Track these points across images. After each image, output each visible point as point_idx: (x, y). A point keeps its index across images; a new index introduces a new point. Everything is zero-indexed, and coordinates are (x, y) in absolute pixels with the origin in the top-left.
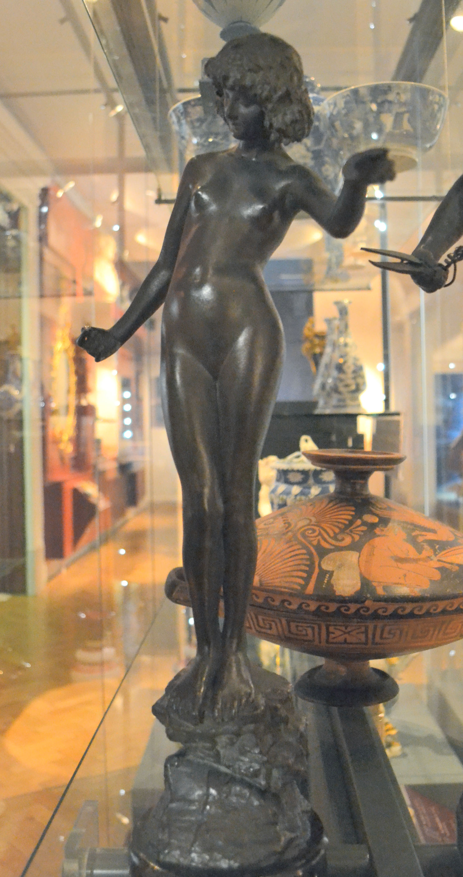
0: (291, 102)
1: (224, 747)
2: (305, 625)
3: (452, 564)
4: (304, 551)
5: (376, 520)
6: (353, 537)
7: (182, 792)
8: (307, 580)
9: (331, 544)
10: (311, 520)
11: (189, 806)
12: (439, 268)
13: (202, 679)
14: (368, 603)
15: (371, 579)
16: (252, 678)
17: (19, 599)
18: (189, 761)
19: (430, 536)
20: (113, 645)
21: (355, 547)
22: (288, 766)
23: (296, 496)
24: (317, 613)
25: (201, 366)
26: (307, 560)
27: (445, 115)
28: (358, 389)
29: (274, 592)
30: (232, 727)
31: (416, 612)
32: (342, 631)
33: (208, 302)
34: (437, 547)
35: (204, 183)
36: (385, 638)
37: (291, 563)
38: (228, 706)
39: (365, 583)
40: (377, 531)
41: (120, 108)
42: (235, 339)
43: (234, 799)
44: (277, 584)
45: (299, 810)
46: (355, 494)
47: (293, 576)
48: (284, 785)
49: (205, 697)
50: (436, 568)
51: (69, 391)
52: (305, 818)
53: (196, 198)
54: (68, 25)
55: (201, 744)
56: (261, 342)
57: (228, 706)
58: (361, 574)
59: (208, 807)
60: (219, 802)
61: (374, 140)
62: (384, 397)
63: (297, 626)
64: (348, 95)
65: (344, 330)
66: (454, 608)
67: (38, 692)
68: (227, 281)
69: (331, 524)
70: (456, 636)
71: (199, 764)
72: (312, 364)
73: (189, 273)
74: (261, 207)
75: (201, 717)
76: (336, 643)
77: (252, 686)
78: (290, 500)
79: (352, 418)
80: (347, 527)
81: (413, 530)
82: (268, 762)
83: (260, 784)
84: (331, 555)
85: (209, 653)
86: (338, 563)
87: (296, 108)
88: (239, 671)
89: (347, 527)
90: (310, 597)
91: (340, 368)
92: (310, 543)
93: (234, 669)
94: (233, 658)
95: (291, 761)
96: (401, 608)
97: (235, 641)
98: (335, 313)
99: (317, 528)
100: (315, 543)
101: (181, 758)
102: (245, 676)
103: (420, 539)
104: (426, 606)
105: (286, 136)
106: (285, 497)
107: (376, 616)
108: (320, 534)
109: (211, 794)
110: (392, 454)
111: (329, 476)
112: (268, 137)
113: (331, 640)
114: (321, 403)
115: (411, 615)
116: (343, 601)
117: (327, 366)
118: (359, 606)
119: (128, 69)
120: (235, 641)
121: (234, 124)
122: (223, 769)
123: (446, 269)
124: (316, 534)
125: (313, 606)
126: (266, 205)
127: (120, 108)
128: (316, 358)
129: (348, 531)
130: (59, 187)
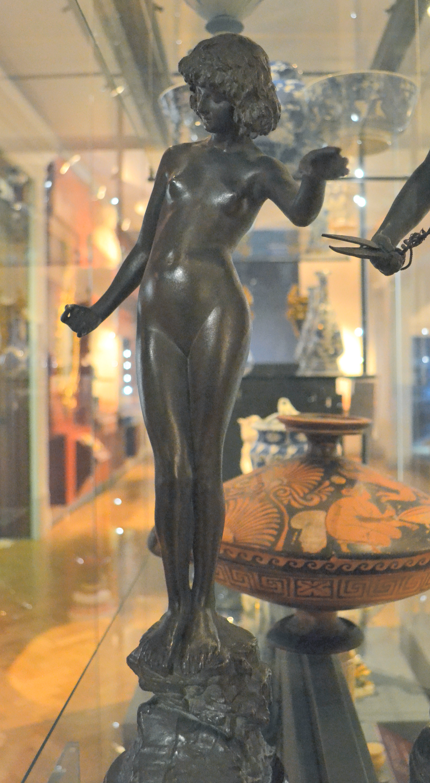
0: (258, 98)
1: (192, 697)
2: (276, 579)
3: (413, 523)
4: (276, 510)
5: (343, 481)
6: (321, 498)
7: (152, 738)
8: (277, 537)
10: (283, 482)
11: (159, 750)
12: (397, 253)
13: (172, 632)
14: (333, 560)
15: (336, 537)
16: (219, 632)
17: (23, 543)
18: (160, 709)
19: (394, 497)
20: (109, 588)
21: (324, 506)
22: (251, 715)
23: (274, 455)
24: (287, 568)
25: (172, 342)
26: (278, 518)
27: (415, 101)
28: (337, 354)
29: (246, 548)
30: (198, 678)
31: (378, 568)
33: (181, 284)
34: (399, 507)
35: (178, 174)
36: (349, 593)
37: (263, 522)
38: (196, 658)
39: (331, 541)
40: (344, 491)
41: (120, 90)
42: (205, 318)
43: (201, 745)
44: (250, 541)
45: (261, 756)
46: (325, 456)
47: (264, 534)
48: (247, 733)
49: (174, 651)
50: (396, 527)
51: (72, 352)
52: (268, 763)
53: (171, 185)
54: (70, 15)
55: (170, 694)
56: (229, 321)
57: (196, 658)
58: (327, 532)
59: (177, 752)
60: (187, 748)
62: (362, 360)
63: (268, 581)
64: (325, 84)
65: (324, 298)
66: (413, 564)
67: (39, 631)
68: (199, 264)
70: (415, 591)
71: (168, 712)
72: (295, 328)
73: (163, 256)
74: (230, 195)
75: (170, 670)
76: (303, 596)
77: (219, 640)
78: (268, 459)
79: (332, 381)
80: (316, 487)
81: (378, 491)
82: (232, 711)
83: (225, 731)
84: (300, 514)
85: (179, 609)
87: (262, 104)
88: (207, 626)
89: (316, 487)
90: (279, 554)
91: (320, 334)
92: (281, 502)
93: (202, 625)
94: (201, 614)
95: (254, 711)
96: (364, 564)
97: (203, 599)
98: (315, 282)
99: (288, 489)
100: (286, 502)
101: (152, 706)
102: (212, 630)
103: (384, 500)
104: (387, 563)
105: (254, 130)
106: (264, 456)
107: (340, 572)
108: (291, 494)
109: (180, 741)
110: (358, 419)
111: (302, 437)
112: (238, 130)
114: (303, 365)
115: (373, 572)
116: (310, 557)
117: (309, 331)
118: (325, 562)
119: (127, 53)
120: (203, 599)
121: (205, 118)
122: (191, 717)
123: (402, 253)
124: (288, 493)
125: (282, 562)
126: (235, 194)
127: (120, 90)
128: (299, 323)
129: (316, 491)
130: (63, 161)
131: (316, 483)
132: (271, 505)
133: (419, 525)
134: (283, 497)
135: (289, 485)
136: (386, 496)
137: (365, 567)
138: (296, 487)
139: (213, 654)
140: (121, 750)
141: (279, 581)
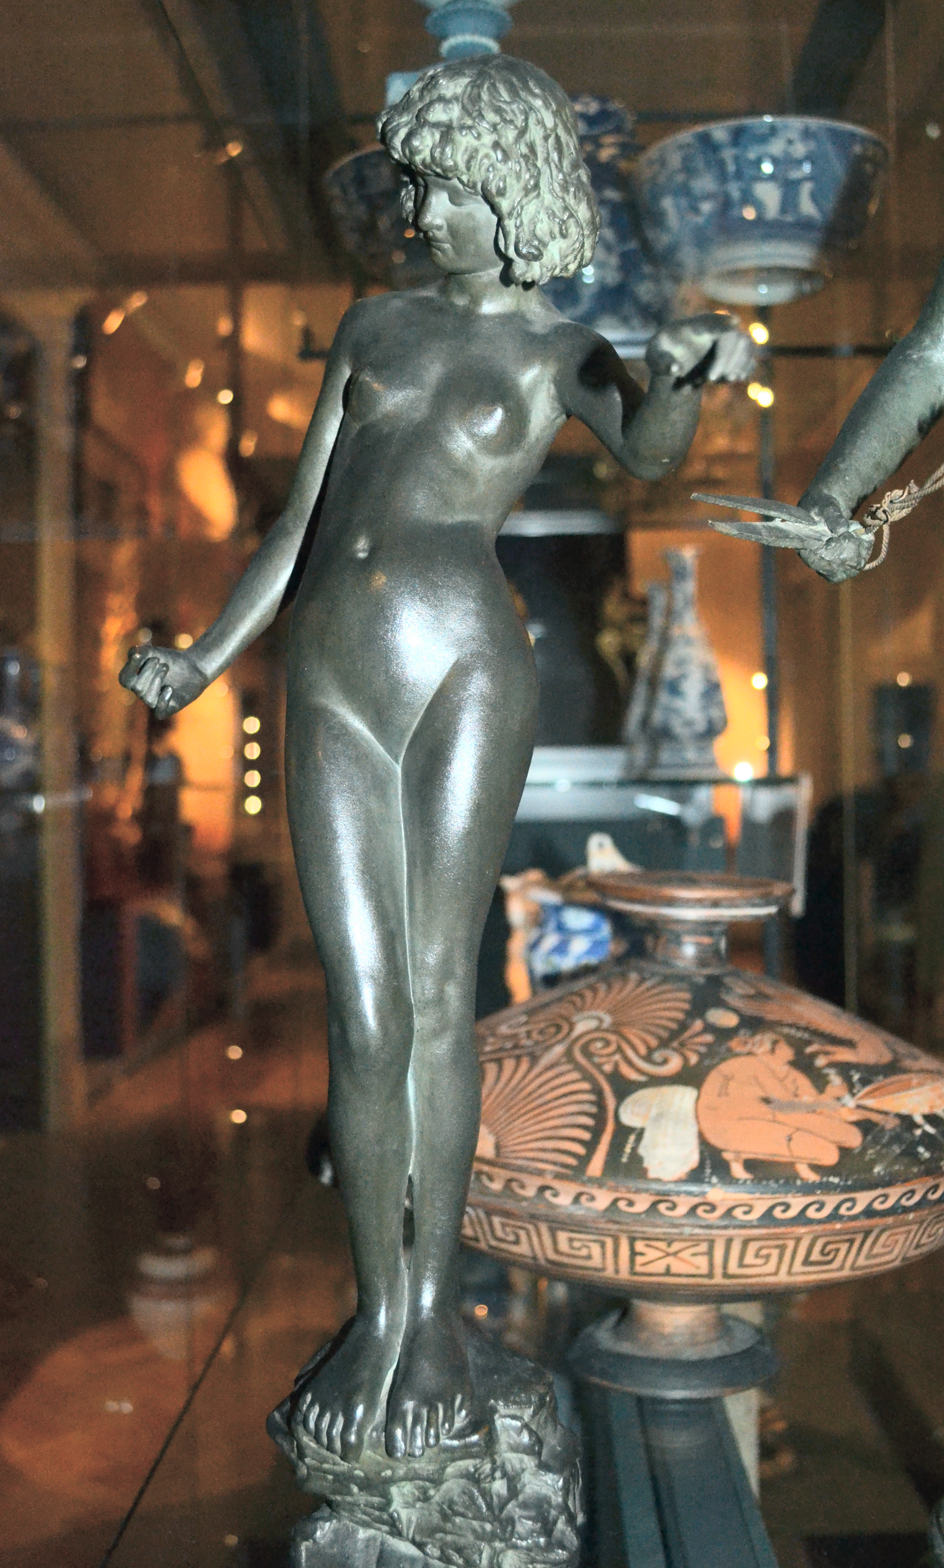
3: (886, 1113)
4: (586, 1086)
6: (686, 1060)
19: (844, 1055)
26: (592, 1103)
31: (811, 1213)
34: (856, 1077)
40: (734, 1044)
41: (234, 150)
63: (571, 1240)
69: (643, 1030)
80: (675, 1035)
86: (654, 1112)
92: (599, 1067)
99: (613, 1038)
100: (608, 1068)
103: (820, 1062)
108: (619, 1050)
113: (638, 1269)
124: (612, 1048)
129: (675, 1044)
131: (674, 1026)
132: (575, 1075)
133: (899, 1116)
134: (602, 1056)
136: (827, 1053)
137: (784, 1211)
138: (631, 1033)
139: (357, 370)
141: (595, 1241)
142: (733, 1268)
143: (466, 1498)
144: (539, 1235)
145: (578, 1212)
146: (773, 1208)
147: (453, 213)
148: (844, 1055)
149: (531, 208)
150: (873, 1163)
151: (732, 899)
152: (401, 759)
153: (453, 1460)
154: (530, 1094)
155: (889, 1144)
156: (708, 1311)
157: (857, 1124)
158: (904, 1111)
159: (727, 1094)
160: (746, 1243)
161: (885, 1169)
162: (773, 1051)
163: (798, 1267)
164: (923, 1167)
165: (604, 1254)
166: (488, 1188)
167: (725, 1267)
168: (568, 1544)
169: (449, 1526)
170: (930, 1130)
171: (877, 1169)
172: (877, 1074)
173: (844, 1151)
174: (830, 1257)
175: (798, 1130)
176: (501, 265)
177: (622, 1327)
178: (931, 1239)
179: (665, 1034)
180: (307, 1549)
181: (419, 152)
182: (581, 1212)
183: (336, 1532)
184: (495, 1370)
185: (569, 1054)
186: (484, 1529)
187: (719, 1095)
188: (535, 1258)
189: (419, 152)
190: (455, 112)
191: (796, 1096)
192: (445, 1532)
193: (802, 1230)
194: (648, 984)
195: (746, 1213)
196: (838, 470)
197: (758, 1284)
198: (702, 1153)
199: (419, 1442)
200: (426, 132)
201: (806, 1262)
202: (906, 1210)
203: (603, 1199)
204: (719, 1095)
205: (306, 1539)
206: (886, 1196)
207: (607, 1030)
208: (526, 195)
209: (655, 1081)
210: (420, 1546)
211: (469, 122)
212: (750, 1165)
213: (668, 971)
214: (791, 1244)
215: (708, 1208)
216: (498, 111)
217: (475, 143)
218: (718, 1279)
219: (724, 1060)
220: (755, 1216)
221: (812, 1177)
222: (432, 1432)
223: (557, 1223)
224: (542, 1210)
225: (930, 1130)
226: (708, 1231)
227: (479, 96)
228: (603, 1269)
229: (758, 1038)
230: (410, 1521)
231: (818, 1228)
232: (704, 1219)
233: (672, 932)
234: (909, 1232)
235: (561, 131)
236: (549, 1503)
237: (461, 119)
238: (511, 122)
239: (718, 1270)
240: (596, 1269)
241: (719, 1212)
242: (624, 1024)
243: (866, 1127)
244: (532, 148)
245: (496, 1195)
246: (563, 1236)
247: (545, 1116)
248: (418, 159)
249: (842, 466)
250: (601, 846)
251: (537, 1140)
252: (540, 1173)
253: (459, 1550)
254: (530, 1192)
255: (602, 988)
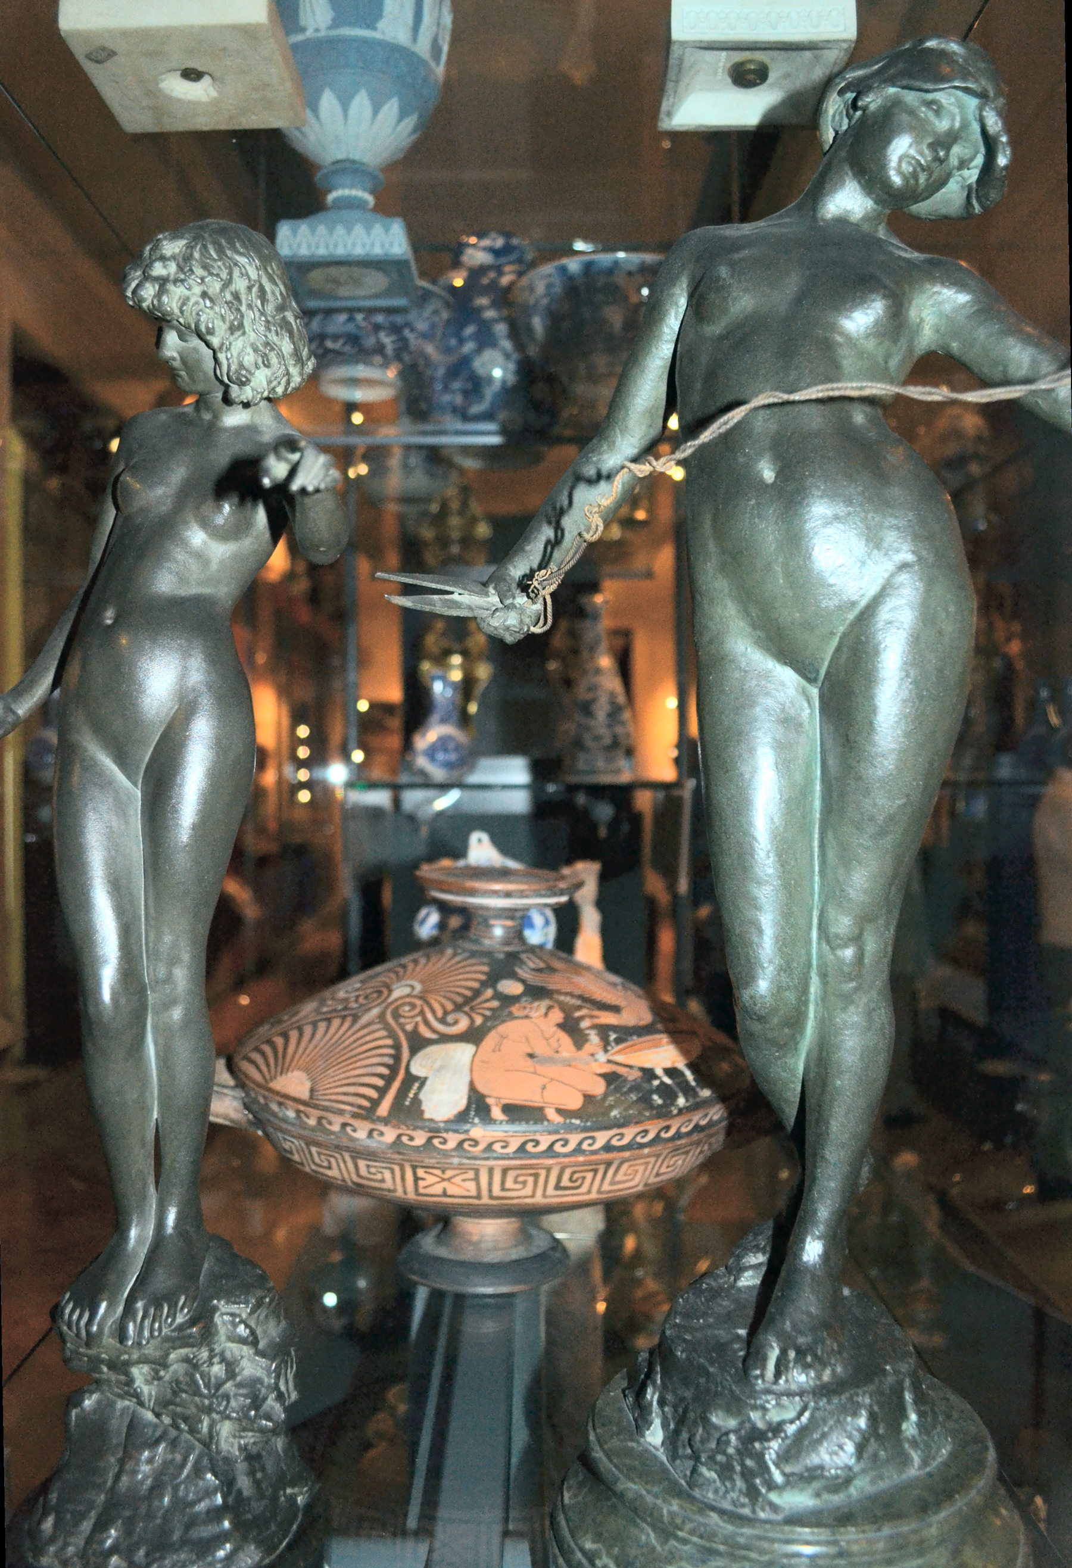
3: (630, 1067)
4: (389, 1042)
6: (472, 1021)
9: (434, 1031)
19: (608, 1018)
21: (473, 1036)
31: (558, 1148)
32: (438, 1176)
34: (613, 1036)
40: (515, 1009)
61: (363, 423)
63: (368, 1166)
69: (444, 997)
80: (468, 1000)
86: (438, 1064)
92: (402, 1026)
99: (418, 1002)
100: (409, 1027)
108: (422, 1013)
113: (422, 1191)
129: (467, 1009)
131: (469, 993)
132: (383, 1033)
133: (643, 1070)
135: (422, 997)
136: (592, 1017)
137: (534, 1146)
140: (1019, 1107)
142: (497, 1191)
143: (188, 1379)
144: (345, 1162)
145: (372, 1144)
146: (525, 1143)
147: (183, 347)
148: (608, 1018)
149: (238, 344)
150: (611, 1107)
151: (522, 891)
152: (140, 786)
153: (175, 1348)
154: (345, 1048)
155: (627, 1093)
156: (508, 1223)
157: (604, 1076)
158: (648, 1065)
159: (499, 1050)
160: (505, 1171)
161: (620, 1113)
162: (546, 1015)
163: (550, 1191)
164: (655, 1112)
165: (394, 1178)
166: (306, 1123)
167: (490, 1191)
168: (275, 1418)
169: (178, 1400)
170: (667, 1080)
171: (614, 1113)
172: (631, 1035)
173: (588, 1098)
174: (578, 1184)
175: (552, 1079)
176: (222, 388)
177: (442, 1236)
178: (669, 1169)
179: (459, 1000)
180: (76, 1416)
181: (144, 300)
182: (375, 1145)
183: (99, 1402)
184: (226, 1276)
185: (382, 1017)
186: (203, 1404)
187: (494, 1051)
188: (344, 1180)
189: (144, 300)
190: (173, 268)
191: (557, 1052)
192: (176, 1405)
193: (550, 1162)
194: (457, 959)
195: (503, 1147)
196: (523, 550)
197: (519, 1205)
198: (469, 1098)
199: (146, 1334)
200: (148, 285)
201: (558, 1187)
202: (642, 1146)
203: (390, 1135)
204: (494, 1051)
205: (75, 1407)
206: (622, 1135)
207: (416, 997)
208: (232, 334)
209: (445, 1039)
210: (158, 1415)
211: (182, 277)
212: (508, 1109)
213: (475, 948)
214: (543, 1173)
215: (472, 1143)
216: (205, 267)
217: (187, 293)
218: (485, 1200)
219: (503, 1021)
220: (511, 1149)
221: (558, 1119)
222: (157, 1325)
223: (358, 1153)
224: (345, 1142)
225: (667, 1080)
226: (473, 1162)
227: (191, 255)
228: (395, 1191)
229: (536, 1004)
230: (150, 1395)
231: (566, 1160)
232: (469, 1152)
233: (481, 916)
234: (647, 1163)
235: (265, 282)
236: (262, 1383)
237: (176, 273)
238: (218, 275)
239: (485, 1193)
240: (389, 1191)
241: (481, 1147)
242: (430, 992)
243: (611, 1078)
244: (236, 296)
245: (313, 1129)
246: (362, 1164)
247: (351, 1067)
248: (144, 305)
249: (528, 548)
250: (480, 840)
251: (342, 1086)
252: (341, 1112)
253: (186, 1420)
254: (336, 1128)
255: (423, 961)
